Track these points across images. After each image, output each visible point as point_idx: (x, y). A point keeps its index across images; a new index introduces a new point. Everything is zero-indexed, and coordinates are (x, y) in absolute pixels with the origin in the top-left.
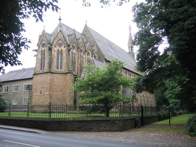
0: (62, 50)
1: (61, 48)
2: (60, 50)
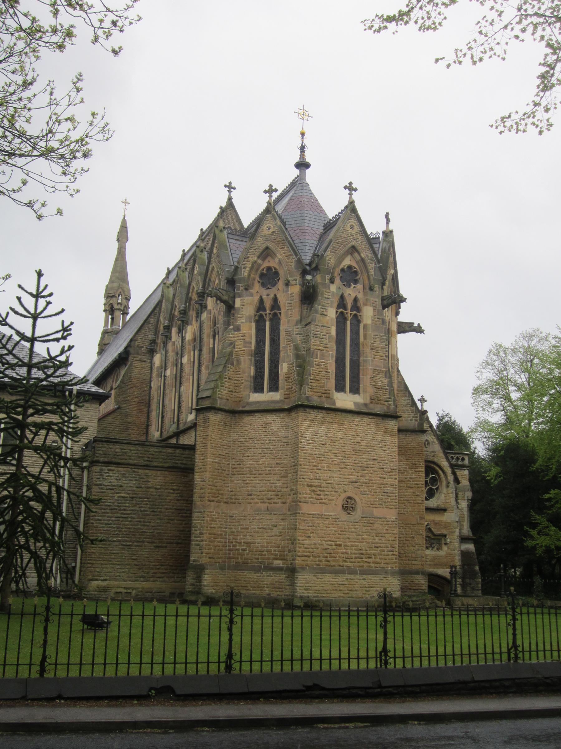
0: (275, 299)
1: (272, 292)
2: (268, 304)
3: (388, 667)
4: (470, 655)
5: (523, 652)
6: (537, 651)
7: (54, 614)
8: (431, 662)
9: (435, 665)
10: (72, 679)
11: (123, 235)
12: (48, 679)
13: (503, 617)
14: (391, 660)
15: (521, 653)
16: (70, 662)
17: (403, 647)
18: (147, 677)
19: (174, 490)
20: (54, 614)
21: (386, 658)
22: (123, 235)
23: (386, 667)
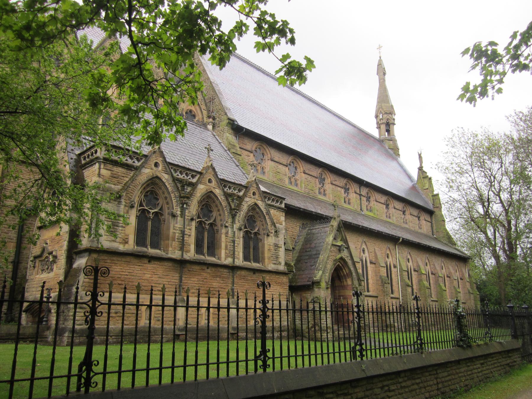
3: (91, 390)
4: (185, 366)
5: (273, 358)
6: (281, 357)
7: (102, 304)
8: (240, 369)
9: (157, 382)
10: (292, 371)
11: (381, 71)
12: (95, 394)
13: (277, 324)
14: (98, 379)
15: (271, 360)
16: (117, 374)
17: (148, 355)
18: (225, 379)
19: (417, 384)
20: (102, 304)
21: (88, 374)
22: (381, 71)
23: (87, 391)
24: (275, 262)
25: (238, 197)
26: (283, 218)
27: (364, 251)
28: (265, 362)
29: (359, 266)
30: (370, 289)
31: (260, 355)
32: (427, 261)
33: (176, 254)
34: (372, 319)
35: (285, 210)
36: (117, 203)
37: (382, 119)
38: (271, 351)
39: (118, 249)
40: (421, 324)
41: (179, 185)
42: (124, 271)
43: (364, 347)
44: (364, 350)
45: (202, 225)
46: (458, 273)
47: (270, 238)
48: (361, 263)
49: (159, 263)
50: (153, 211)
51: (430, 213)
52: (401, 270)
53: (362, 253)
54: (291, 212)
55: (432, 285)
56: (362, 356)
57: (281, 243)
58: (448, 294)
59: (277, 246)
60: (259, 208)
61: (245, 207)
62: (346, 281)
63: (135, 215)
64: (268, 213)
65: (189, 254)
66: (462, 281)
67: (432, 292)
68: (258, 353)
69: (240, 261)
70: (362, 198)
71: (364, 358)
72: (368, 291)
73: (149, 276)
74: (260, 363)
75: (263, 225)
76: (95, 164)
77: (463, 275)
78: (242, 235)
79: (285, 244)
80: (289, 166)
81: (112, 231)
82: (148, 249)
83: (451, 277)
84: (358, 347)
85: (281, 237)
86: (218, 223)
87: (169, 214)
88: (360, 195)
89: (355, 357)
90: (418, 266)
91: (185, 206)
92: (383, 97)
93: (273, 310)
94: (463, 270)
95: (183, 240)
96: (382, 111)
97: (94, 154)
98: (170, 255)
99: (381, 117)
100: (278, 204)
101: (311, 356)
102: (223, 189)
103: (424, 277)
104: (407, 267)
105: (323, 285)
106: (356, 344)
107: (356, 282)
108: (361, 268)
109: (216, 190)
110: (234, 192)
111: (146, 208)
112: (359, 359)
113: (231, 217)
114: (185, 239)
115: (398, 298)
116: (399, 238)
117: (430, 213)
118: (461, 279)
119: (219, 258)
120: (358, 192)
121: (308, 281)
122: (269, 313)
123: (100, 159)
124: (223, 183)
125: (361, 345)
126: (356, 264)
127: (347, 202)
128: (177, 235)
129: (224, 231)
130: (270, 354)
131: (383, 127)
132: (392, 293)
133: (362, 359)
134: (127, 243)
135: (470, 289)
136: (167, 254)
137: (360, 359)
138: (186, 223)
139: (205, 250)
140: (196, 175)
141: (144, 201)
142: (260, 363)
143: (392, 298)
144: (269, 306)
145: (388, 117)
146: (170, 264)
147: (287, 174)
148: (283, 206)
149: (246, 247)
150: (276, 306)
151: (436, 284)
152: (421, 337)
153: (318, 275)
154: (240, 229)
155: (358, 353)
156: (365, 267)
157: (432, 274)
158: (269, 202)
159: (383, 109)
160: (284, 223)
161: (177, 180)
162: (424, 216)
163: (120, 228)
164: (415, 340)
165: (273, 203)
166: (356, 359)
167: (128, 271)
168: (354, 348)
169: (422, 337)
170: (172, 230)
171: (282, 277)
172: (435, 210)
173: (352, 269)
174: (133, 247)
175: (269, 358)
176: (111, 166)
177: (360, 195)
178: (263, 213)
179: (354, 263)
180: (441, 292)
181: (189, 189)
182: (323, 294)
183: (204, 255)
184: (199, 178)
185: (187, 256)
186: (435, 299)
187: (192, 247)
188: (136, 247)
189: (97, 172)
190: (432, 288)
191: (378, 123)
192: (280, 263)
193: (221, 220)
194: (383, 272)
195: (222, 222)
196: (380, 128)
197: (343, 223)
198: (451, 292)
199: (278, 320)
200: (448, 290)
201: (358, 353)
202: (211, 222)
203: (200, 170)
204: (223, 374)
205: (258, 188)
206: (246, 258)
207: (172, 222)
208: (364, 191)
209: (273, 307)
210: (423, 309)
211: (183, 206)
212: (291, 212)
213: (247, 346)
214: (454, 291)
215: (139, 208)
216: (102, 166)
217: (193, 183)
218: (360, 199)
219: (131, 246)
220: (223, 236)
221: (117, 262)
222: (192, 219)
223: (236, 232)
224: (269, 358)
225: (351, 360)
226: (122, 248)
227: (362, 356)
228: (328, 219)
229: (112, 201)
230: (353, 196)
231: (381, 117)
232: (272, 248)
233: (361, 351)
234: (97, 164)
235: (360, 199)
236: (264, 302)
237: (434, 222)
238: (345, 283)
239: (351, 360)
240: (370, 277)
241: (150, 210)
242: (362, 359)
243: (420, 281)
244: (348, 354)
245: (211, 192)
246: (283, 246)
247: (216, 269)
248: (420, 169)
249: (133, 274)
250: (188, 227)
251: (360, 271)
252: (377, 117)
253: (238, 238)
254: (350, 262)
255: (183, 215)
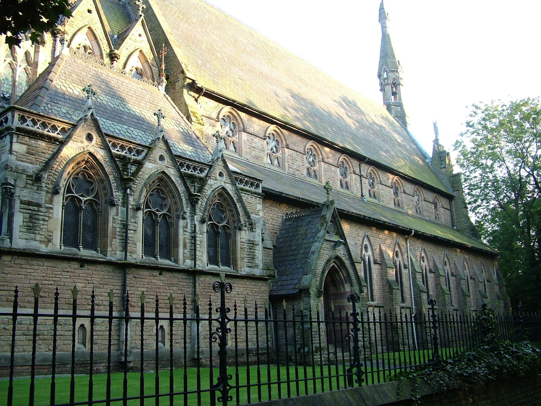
5: (237, 387)
24: (250, 265)
25: (201, 179)
26: (259, 207)
27: (366, 248)
28: (225, 393)
29: (360, 267)
30: (374, 298)
31: (218, 385)
32: (446, 259)
33: (115, 254)
34: (380, 336)
35: (262, 195)
36: (36, 188)
37: (387, 79)
38: (234, 377)
39: (38, 251)
40: (438, 336)
41: (120, 164)
42: (48, 279)
43: (363, 369)
44: (363, 373)
45: (151, 216)
46: (484, 274)
47: (243, 233)
48: (362, 264)
49: (94, 268)
50: (86, 199)
51: (450, 198)
52: (414, 272)
53: (364, 252)
54: (271, 197)
55: (452, 290)
56: (360, 381)
57: (258, 239)
58: (472, 300)
59: (252, 244)
60: (228, 193)
61: (208, 191)
62: (344, 287)
63: (61, 204)
64: (240, 200)
65: (134, 256)
66: (489, 284)
67: (453, 298)
68: (215, 382)
69: (203, 262)
70: (363, 179)
71: (364, 384)
72: (372, 300)
73: (82, 285)
74: (218, 394)
75: (233, 216)
76: (6, 136)
77: (490, 276)
78: (205, 230)
79: (263, 240)
80: (268, 139)
81: (32, 226)
82: (79, 250)
83: (476, 279)
84: (355, 370)
85: (258, 231)
86: (174, 214)
87: (106, 202)
88: (361, 176)
89: (351, 384)
90: (435, 266)
91: (128, 191)
92: (386, 39)
93: (236, 321)
94: (491, 271)
95: (126, 236)
96: (387, 69)
97: (4, 124)
98: (109, 258)
99: (385, 76)
100: (253, 189)
101: (282, 385)
102: (179, 169)
103: (442, 280)
104: (421, 268)
105: (313, 291)
106: (352, 367)
107: (356, 288)
108: (363, 270)
109: (170, 169)
110: (193, 172)
111: (76, 195)
112: (356, 385)
113: (190, 205)
114: (129, 235)
115: (410, 308)
116: (411, 230)
117: (450, 198)
118: (488, 281)
119: (176, 261)
120: (357, 171)
121: (294, 289)
122: (230, 325)
123: (12, 129)
124: (178, 160)
125: (359, 366)
126: (356, 265)
127: (344, 186)
128: (118, 230)
129: (181, 223)
130: (232, 382)
131: (388, 88)
132: (403, 301)
133: (360, 385)
134: (49, 241)
135: (499, 293)
136: (106, 255)
137: (358, 385)
138: (130, 213)
139: (158, 250)
140: (142, 151)
141: (73, 185)
142: (218, 394)
143: (402, 308)
144: (231, 315)
145: (394, 76)
146: (110, 269)
147: (266, 149)
148: (260, 191)
149: (212, 244)
150: (241, 316)
151: (457, 289)
152: (438, 353)
153: (306, 280)
154: (203, 221)
155: (355, 377)
156: (368, 270)
157: (452, 275)
158: (242, 186)
159: (387, 66)
160: (261, 213)
161: (116, 157)
162: (443, 202)
163: (41, 222)
164: (431, 358)
165: (247, 188)
166: (353, 387)
167: (54, 279)
168: (350, 371)
169: (440, 354)
170: (110, 224)
171: (260, 284)
172: (455, 194)
173: (351, 271)
174: (59, 247)
175: (231, 387)
176: (27, 138)
177: (361, 176)
178: (233, 200)
179: (353, 263)
180: (464, 295)
181: (134, 168)
182: (317, 305)
183: (155, 257)
184: (146, 154)
185: (130, 259)
186: (456, 307)
187: (140, 246)
188: (62, 247)
189: (8, 148)
190: (453, 294)
191: (381, 84)
192: (257, 266)
193: (177, 210)
194: (392, 273)
195: (178, 213)
196: (384, 90)
197: (339, 213)
198: (477, 299)
199: (246, 337)
200: (472, 296)
201: (355, 377)
202: (164, 212)
203: (148, 145)
204: (265, 398)
205: (226, 167)
206: (212, 260)
207: (112, 212)
208: (366, 169)
209: (235, 317)
210: (440, 317)
211: (125, 192)
212: (271, 197)
213: (172, 374)
214: (479, 297)
215: (66, 196)
216: (15, 139)
217: (138, 161)
218: (361, 181)
219: (57, 245)
220: (181, 231)
221: (37, 267)
222: (138, 209)
223: (197, 226)
224: (231, 387)
225: (346, 388)
226: (44, 249)
227: (360, 381)
228: (318, 207)
229: (28, 186)
230: (353, 179)
231: (385, 76)
232: (246, 246)
233: (359, 373)
234: (8, 137)
235: (361, 181)
236: (223, 310)
237: (454, 209)
238: (342, 290)
239: (346, 388)
240: (374, 281)
241: (81, 198)
242: (360, 385)
243: (437, 284)
244: (341, 379)
245: (163, 172)
246: (260, 243)
247: (172, 275)
248: (436, 141)
249: (59, 283)
250: (132, 220)
251: (361, 274)
252: (380, 76)
253: (201, 234)
254: (347, 263)
255: (125, 203)
